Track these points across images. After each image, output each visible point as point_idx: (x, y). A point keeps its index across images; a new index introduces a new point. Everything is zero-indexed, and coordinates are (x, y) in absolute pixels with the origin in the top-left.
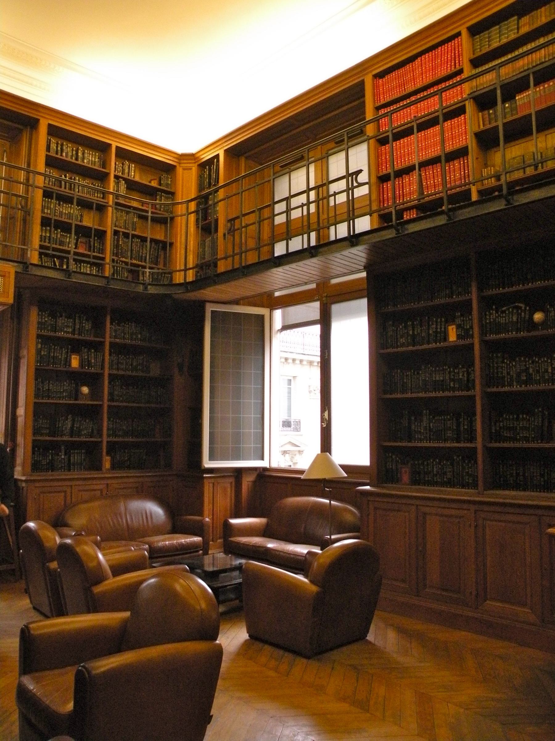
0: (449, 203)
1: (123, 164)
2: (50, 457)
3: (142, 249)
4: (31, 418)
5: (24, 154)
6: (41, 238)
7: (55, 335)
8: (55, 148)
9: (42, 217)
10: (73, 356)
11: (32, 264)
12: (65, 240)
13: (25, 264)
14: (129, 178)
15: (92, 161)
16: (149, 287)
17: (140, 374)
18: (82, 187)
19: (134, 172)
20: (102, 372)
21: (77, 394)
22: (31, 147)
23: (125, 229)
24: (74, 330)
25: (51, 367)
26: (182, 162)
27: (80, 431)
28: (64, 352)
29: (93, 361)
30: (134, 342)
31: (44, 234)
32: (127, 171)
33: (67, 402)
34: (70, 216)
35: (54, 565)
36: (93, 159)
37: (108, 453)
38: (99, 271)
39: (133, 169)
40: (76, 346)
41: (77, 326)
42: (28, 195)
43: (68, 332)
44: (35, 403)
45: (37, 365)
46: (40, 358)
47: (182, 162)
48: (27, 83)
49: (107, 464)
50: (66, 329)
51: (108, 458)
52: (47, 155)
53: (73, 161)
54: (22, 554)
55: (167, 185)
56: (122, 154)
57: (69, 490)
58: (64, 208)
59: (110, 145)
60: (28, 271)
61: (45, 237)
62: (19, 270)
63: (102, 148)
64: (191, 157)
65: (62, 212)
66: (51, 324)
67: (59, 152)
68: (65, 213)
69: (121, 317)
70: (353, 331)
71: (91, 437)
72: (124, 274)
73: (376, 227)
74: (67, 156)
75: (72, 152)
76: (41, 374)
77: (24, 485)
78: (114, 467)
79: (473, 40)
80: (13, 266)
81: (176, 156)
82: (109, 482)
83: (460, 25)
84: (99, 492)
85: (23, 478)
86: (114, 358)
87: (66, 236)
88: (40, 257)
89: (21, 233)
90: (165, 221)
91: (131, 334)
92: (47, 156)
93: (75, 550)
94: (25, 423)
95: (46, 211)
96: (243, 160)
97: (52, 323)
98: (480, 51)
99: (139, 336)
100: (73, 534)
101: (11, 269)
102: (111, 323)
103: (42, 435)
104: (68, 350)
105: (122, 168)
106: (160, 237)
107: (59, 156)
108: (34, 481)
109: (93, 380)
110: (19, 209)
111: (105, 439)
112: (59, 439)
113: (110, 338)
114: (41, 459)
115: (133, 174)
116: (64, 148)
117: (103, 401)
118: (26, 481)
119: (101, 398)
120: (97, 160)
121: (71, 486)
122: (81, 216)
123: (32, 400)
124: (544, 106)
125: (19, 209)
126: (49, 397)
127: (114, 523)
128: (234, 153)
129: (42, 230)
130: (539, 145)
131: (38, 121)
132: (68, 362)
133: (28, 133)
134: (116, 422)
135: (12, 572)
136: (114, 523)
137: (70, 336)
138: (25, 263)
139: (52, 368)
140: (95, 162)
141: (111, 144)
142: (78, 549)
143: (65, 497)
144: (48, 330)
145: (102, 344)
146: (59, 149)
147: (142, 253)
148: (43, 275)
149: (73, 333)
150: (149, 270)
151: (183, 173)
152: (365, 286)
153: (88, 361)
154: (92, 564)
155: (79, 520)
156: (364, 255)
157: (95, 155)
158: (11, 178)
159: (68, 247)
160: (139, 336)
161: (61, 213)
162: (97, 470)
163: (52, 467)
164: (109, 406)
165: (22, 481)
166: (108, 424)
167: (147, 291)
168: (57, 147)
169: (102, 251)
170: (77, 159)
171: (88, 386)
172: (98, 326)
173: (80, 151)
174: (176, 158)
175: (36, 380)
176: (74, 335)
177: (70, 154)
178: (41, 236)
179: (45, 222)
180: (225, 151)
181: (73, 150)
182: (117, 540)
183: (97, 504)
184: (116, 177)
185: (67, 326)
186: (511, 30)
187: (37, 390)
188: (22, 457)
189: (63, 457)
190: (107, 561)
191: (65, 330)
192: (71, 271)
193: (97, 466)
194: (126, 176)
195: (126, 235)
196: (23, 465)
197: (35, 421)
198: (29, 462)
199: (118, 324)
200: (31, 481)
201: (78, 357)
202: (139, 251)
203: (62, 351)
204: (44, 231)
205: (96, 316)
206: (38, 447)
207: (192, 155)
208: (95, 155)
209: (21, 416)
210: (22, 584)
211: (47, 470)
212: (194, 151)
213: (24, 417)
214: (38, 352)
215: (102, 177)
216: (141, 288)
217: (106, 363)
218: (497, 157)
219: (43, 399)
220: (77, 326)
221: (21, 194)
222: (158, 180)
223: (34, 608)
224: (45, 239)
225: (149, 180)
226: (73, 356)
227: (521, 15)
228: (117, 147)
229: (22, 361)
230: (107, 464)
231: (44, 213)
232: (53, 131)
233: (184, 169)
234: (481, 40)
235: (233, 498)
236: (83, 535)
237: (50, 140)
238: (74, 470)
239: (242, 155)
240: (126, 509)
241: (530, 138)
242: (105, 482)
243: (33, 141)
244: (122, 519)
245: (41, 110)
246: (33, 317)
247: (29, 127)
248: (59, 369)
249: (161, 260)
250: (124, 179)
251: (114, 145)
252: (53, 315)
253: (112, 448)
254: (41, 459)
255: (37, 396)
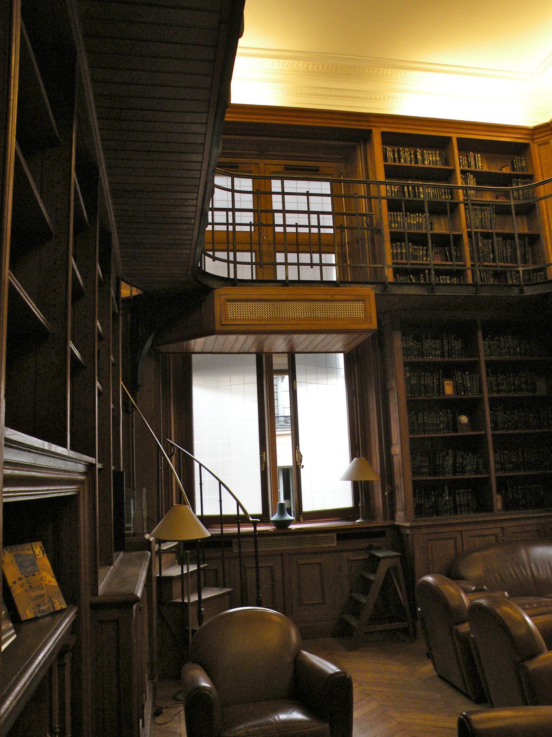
1: (467, 157)
2: (433, 500)
3: (506, 249)
4: (408, 457)
5: (361, 171)
6: (393, 256)
7: (423, 360)
8: (392, 156)
10: (446, 382)
11: (390, 283)
12: (418, 254)
13: (384, 285)
14: (477, 170)
15: (433, 161)
16: (525, 288)
17: (525, 394)
18: (427, 192)
19: (481, 163)
20: (480, 396)
21: (455, 425)
22: (367, 162)
23: (482, 228)
24: (443, 353)
25: (423, 397)
26: (535, 137)
27: (463, 467)
28: (435, 378)
29: (469, 385)
30: (513, 358)
31: (395, 251)
32: (473, 163)
33: (445, 435)
34: (419, 225)
35: (465, 628)
36: (434, 158)
37: (498, 491)
38: (460, 280)
39: (480, 159)
40: (448, 370)
41: (446, 348)
42: (371, 211)
43: (437, 356)
44: (411, 439)
45: (408, 397)
46: (411, 389)
47: (535, 137)
48: (353, 98)
49: (498, 504)
50: (433, 352)
51: (499, 497)
52: (385, 165)
53: (413, 164)
54: (421, 612)
55: (522, 169)
56: (467, 146)
57: (458, 537)
58: (412, 219)
59: (450, 138)
60: (387, 292)
61: (397, 253)
62: (378, 292)
63: (440, 144)
65: (410, 223)
66: (418, 349)
67: (397, 159)
68: (414, 224)
69: (493, 330)
71: (476, 473)
72: (489, 280)
74: (405, 162)
75: (411, 157)
76: (414, 407)
77: (408, 532)
78: (507, 507)
80: (373, 288)
82: (504, 524)
84: (494, 537)
85: (408, 525)
86: (493, 379)
87: (419, 249)
88: (395, 276)
89: (371, 254)
91: (508, 348)
92: (386, 166)
93: (496, 612)
94: (403, 464)
95: (393, 226)
97: (418, 347)
99: (518, 350)
100: (473, 588)
101: (369, 291)
102: (484, 339)
103: (422, 474)
104: (439, 376)
105: (468, 160)
106: (525, 230)
107: (397, 164)
108: (420, 527)
109: (471, 407)
110: (365, 229)
111: (493, 475)
112: (442, 478)
113: (485, 356)
114: (423, 502)
115: (480, 165)
116: (402, 153)
117: (485, 430)
118: (410, 528)
119: (484, 428)
120: (438, 159)
121: (461, 531)
122: (431, 224)
123: (407, 436)
125: (365, 229)
126: (424, 431)
127: (516, 574)
129: (392, 247)
132: (440, 389)
133: (362, 147)
134: (503, 454)
135: (405, 631)
136: (516, 574)
137: (439, 359)
138: (384, 283)
139: (425, 398)
140: (436, 161)
141: (451, 137)
142: (498, 611)
143: (455, 543)
144: (415, 356)
145: (477, 363)
146: (396, 156)
147: (507, 253)
148: (403, 293)
149: (443, 356)
150: (522, 269)
153: (464, 385)
154: (521, 632)
155: (474, 571)
157: (435, 153)
158: (356, 194)
159: (423, 260)
160: (518, 350)
161: (410, 225)
162: (487, 511)
163: (436, 511)
164: (493, 435)
165: (406, 527)
166: (495, 457)
167: (523, 293)
168: (394, 155)
169: (461, 258)
170: (416, 162)
171: (465, 414)
172: (470, 345)
173: (418, 153)
174: (528, 135)
175: (409, 413)
176: (444, 358)
177: (409, 159)
178: (392, 253)
179: (396, 238)
181: (410, 154)
182: (527, 595)
183: (492, 551)
184: (463, 172)
185: (436, 349)
187: (411, 424)
188: (403, 501)
189: (447, 498)
190: (536, 624)
191: (433, 353)
192: (434, 284)
193: (485, 506)
194: (473, 168)
195: (487, 236)
196: (405, 510)
197: (413, 459)
198: (411, 506)
199: (492, 340)
200: (415, 527)
201: (451, 382)
202: (503, 250)
203: (433, 378)
204: (394, 248)
205: (465, 332)
206: (420, 489)
208: (435, 153)
209: (397, 455)
210: (421, 645)
211: (430, 515)
213: (400, 456)
214: (408, 381)
215: (448, 176)
216: (515, 292)
217: (485, 387)
219: (418, 434)
220: (446, 348)
221: (364, 212)
222: (510, 165)
223: (440, 677)
224: (397, 256)
225: (499, 168)
226: (446, 382)
228: (458, 139)
229: (391, 394)
230: (498, 504)
231: (392, 228)
232: (389, 139)
233: (539, 145)
236: (484, 590)
237: (386, 149)
238: (462, 512)
240: (528, 555)
242: (499, 525)
243: (368, 155)
244: (525, 569)
245: (372, 120)
246: (398, 342)
247: (362, 142)
248: (431, 398)
249: (529, 257)
250: (472, 172)
251: (454, 137)
252: (418, 339)
253: (503, 485)
254: (423, 502)
255: (412, 431)
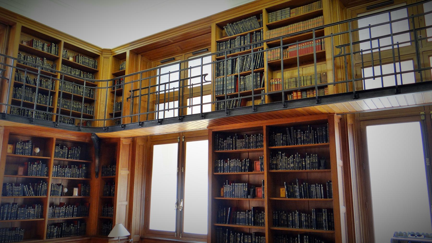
0: (254, 94)
9: (15, 82)
56: (68, 46)
64: (110, 51)
70: (199, 152)
73: (214, 111)
79: (268, 15)
81: (100, 50)
83: (262, 7)
90: (93, 86)
96: (140, 57)
98: (272, 21)
124: (302, 55)
128: (136, 53)
130: (301, 72)
131: (15, 24)
151: (104, 60)
152: (207, 134)
156: (208, 122)
180: (131, 51)
186: (287, 14)
207: (110, 50)
212: (111, 48)
218: (278, 75)
227: (292, 8)
228: (65, 42)
232: (25, 30)
234: (272, 16)
235: (101, 76)
239: (140, 54)
241: (296, 68)
251: (63, 41)
